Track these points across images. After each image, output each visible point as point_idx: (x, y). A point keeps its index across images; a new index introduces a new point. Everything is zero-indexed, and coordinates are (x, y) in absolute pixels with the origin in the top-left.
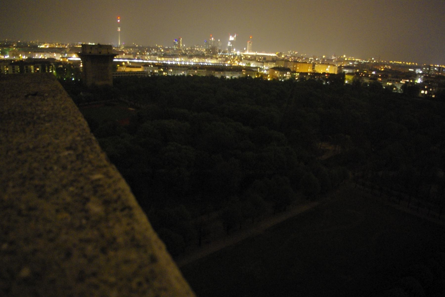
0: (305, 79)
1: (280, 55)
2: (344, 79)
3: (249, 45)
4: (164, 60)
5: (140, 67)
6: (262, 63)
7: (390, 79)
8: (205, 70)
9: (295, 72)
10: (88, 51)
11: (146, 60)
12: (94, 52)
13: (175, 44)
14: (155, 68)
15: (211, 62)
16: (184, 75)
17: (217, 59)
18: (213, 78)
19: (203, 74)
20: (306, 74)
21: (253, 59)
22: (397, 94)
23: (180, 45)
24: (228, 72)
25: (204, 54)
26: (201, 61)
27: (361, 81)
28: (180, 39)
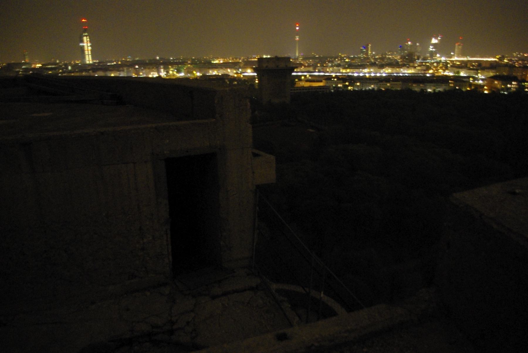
4: (349, 72)
5: (321, 81)
6: (475, 71)
13: (363, 52)
14: (338, 81)
16: (373, 89)
17: (415, 67)
18: (410, 92)
19: (398, 87)
25: (397, 63)
26: (394, 71)
28: (368, 45)
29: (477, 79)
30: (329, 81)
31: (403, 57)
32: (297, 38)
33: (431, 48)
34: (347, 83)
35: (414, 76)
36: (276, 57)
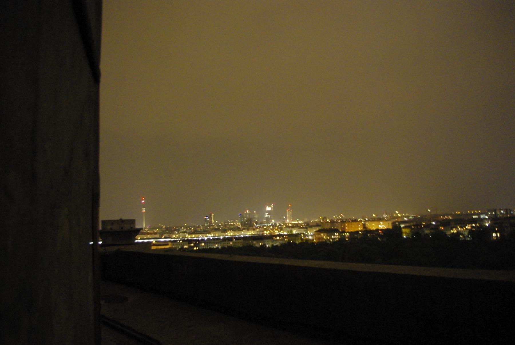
0: (357, 238)
1: (324, 218)
2: (401, 233)
3: (289, 213)
4: (194, 237)
5: (167, 245)
7: (453, 226)
8: (242, 241)
9: (344, 232)
10: (109, 227)
11: (174, 238)
12: (116, 228)
13: (207, 222)
14: (184, 243)
15: (249, 233)
16: (217, 248)
17: (254, 230)
19: (240, 244)
20: (357, 232)
21: (294, 226)
22: (465, 241)
23: (212, 222)
24: (268, 240)
25: (239, 228)
26: (236, 234)
27: (420, 232)
28: (211, 215)
29: (308, 236)
30: (175, 244)
31: (243, 224)
32: (144, 210)
33: (266, 215)
34: (192, 245)
35: (254, 237)
36: (121, 219)
